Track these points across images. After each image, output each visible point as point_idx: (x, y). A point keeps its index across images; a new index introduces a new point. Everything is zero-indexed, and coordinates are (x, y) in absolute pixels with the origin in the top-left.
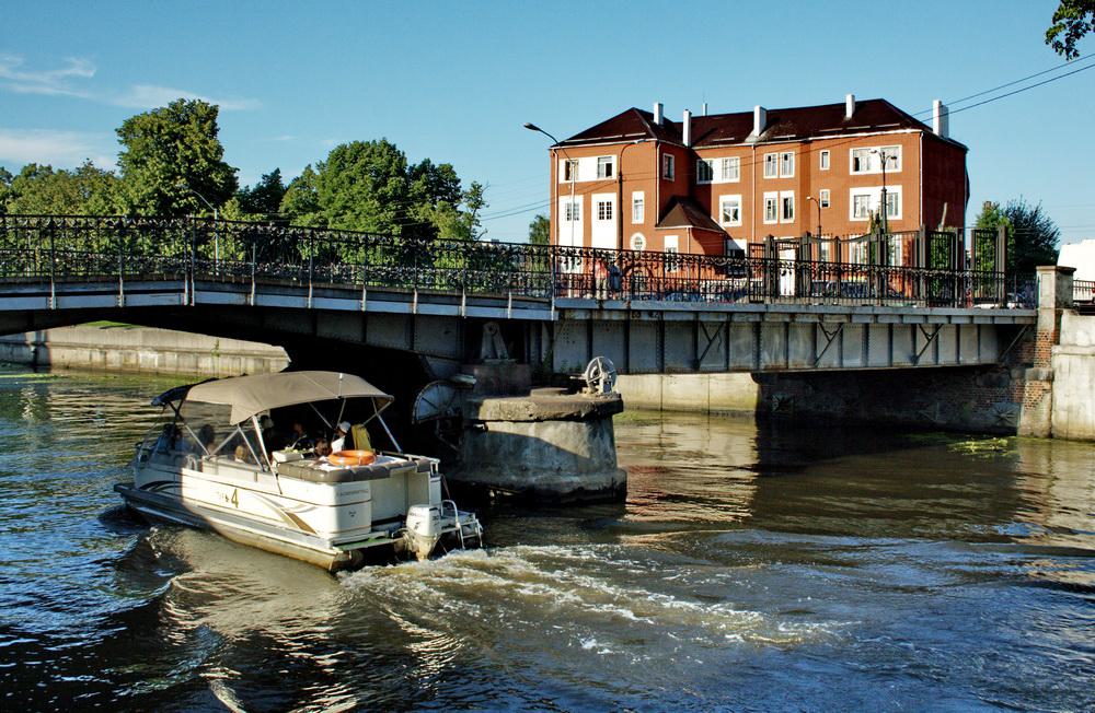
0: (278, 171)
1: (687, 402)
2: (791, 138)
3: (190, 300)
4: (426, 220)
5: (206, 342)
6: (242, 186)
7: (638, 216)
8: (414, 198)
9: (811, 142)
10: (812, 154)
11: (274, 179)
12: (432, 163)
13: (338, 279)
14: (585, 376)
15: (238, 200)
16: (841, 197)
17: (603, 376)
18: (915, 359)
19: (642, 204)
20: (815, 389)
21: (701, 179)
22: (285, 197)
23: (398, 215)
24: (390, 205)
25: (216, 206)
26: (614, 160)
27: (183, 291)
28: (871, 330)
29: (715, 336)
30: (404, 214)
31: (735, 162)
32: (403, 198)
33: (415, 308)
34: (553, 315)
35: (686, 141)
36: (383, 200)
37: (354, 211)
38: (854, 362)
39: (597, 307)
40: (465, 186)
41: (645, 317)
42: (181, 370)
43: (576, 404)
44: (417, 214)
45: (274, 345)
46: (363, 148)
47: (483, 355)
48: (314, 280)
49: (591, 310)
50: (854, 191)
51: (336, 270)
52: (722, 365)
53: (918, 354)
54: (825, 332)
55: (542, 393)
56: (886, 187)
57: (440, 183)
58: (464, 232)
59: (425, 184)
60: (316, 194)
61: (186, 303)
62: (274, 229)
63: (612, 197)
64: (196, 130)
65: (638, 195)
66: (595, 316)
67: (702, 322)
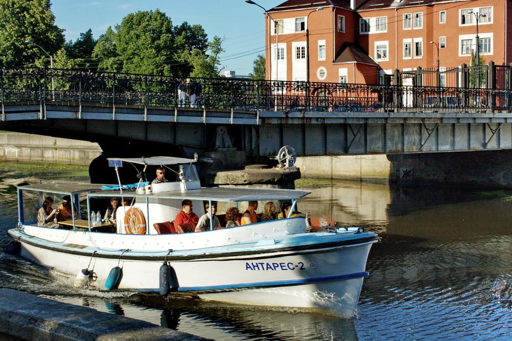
0: (90, 31)
1: (348, 174)
2: (421, 3)
3: (43, 116)
4: (186, 61)
5: (48, 141)
6: (67, 41)
7: (322, 56)
8: (178, 48)
9: (433, 6)
10: (435, 14)
11: (88, 36)
12: (188, 25)
13: (132, 102)
14: (277, 157)
15: (66, 49)
16: (453, 40)
17: (288, 157)
18: (485, 145)
19: (324, 46)
20: (426, 164)
21: (362, 31)
22: (96, 47)
23: (168, 58)
24: (163, 52)
25: (51, 54)
26: (305, 20)
27: (39, 111)
28: (456, 127)
29: (357, 133)
30: (171, 58)
31: (384, 19)
32: (171, 47)
33: (175, 118)
34: (258, 121)
35: (352, 6)
36: (158, 49)
37: (140, 56)
38: (445, 148)
39: (284, 116)
40: (210, 39)
41: (314, 122)
42: (32, 159)
43: (272, 174)
44: (179, 58)
45: (92, 142)
46: (144, 15)
47: (217, 146)
48: (116, 103)
49: (281, 118)
50: (461, 37)
51: (128, 95)
52: (363, 150)
53: (486, 142)
54: (427, 129)
55: (251, 168)
56: (479, 35)
57: (194, 36)
58: (209, 68)
59: (184, 38)
60: (115, 45)
61: (41, 118)
62: (91, 74)
63: (303, 44)
64: (37, 5)
65: (322, 42)
66: (284, 122)
67: (349, 124)
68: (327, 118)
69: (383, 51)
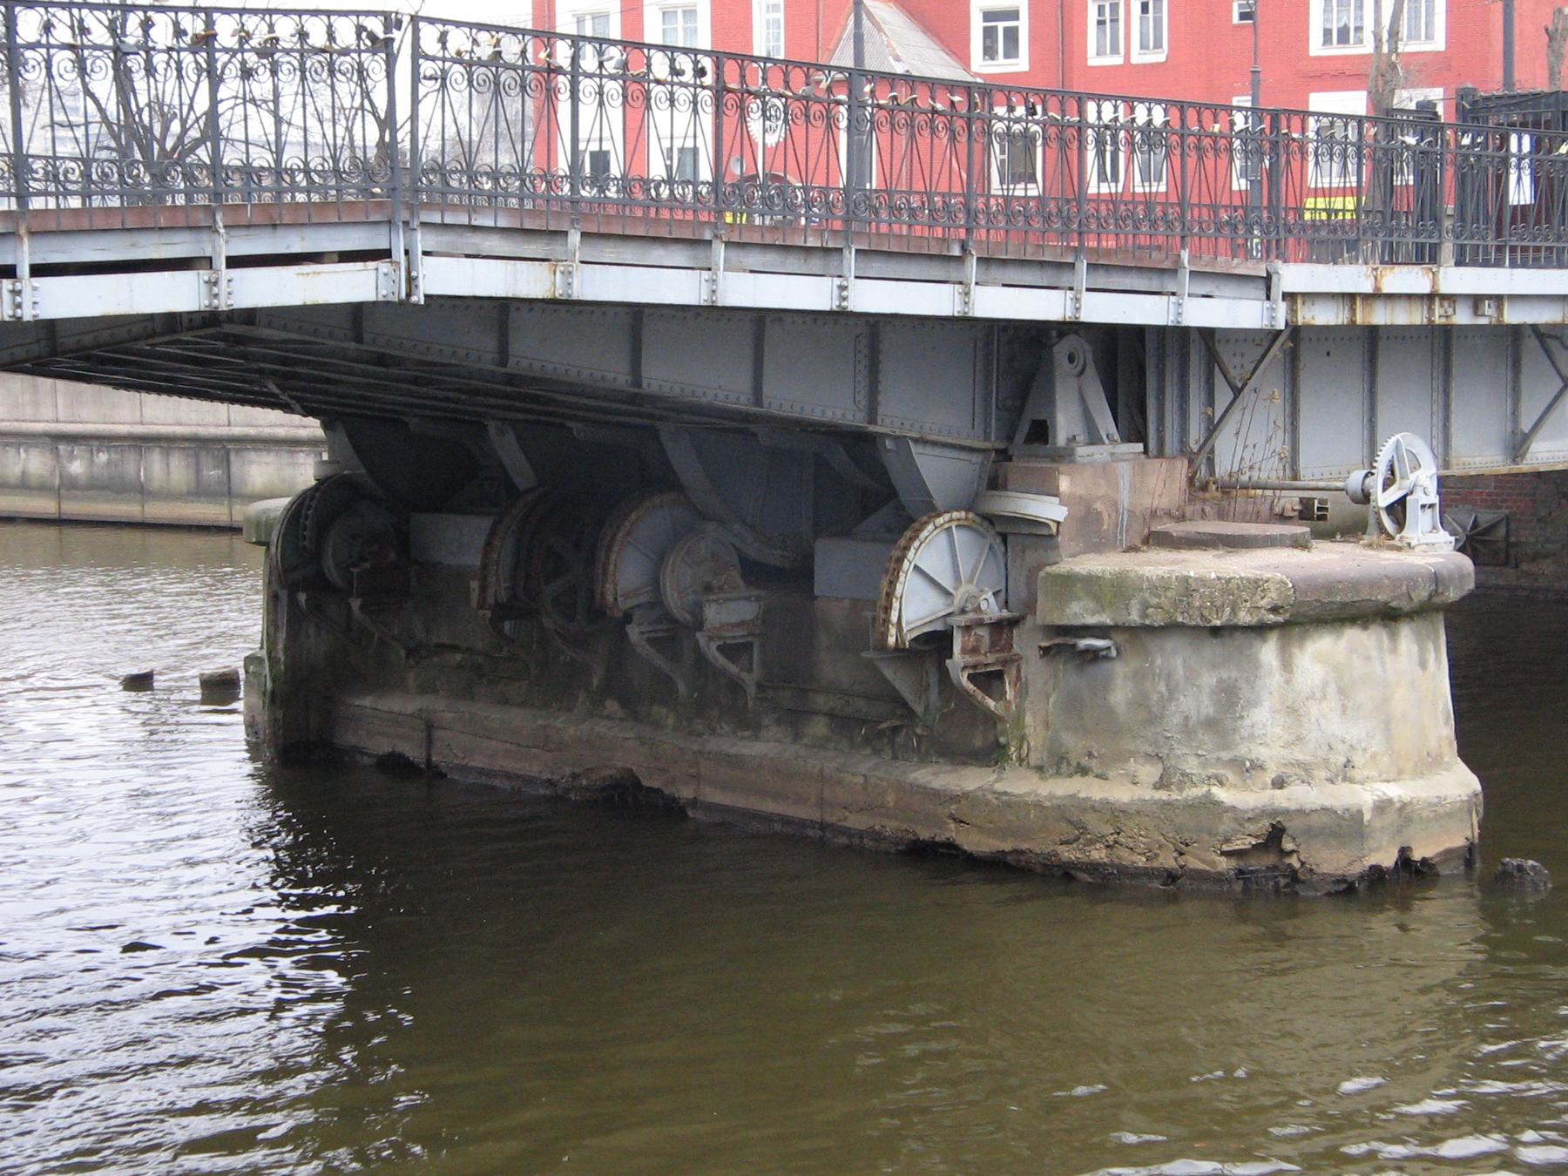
53: (1526, 426)
68: (1305, 295)
69: (1006, 30)
